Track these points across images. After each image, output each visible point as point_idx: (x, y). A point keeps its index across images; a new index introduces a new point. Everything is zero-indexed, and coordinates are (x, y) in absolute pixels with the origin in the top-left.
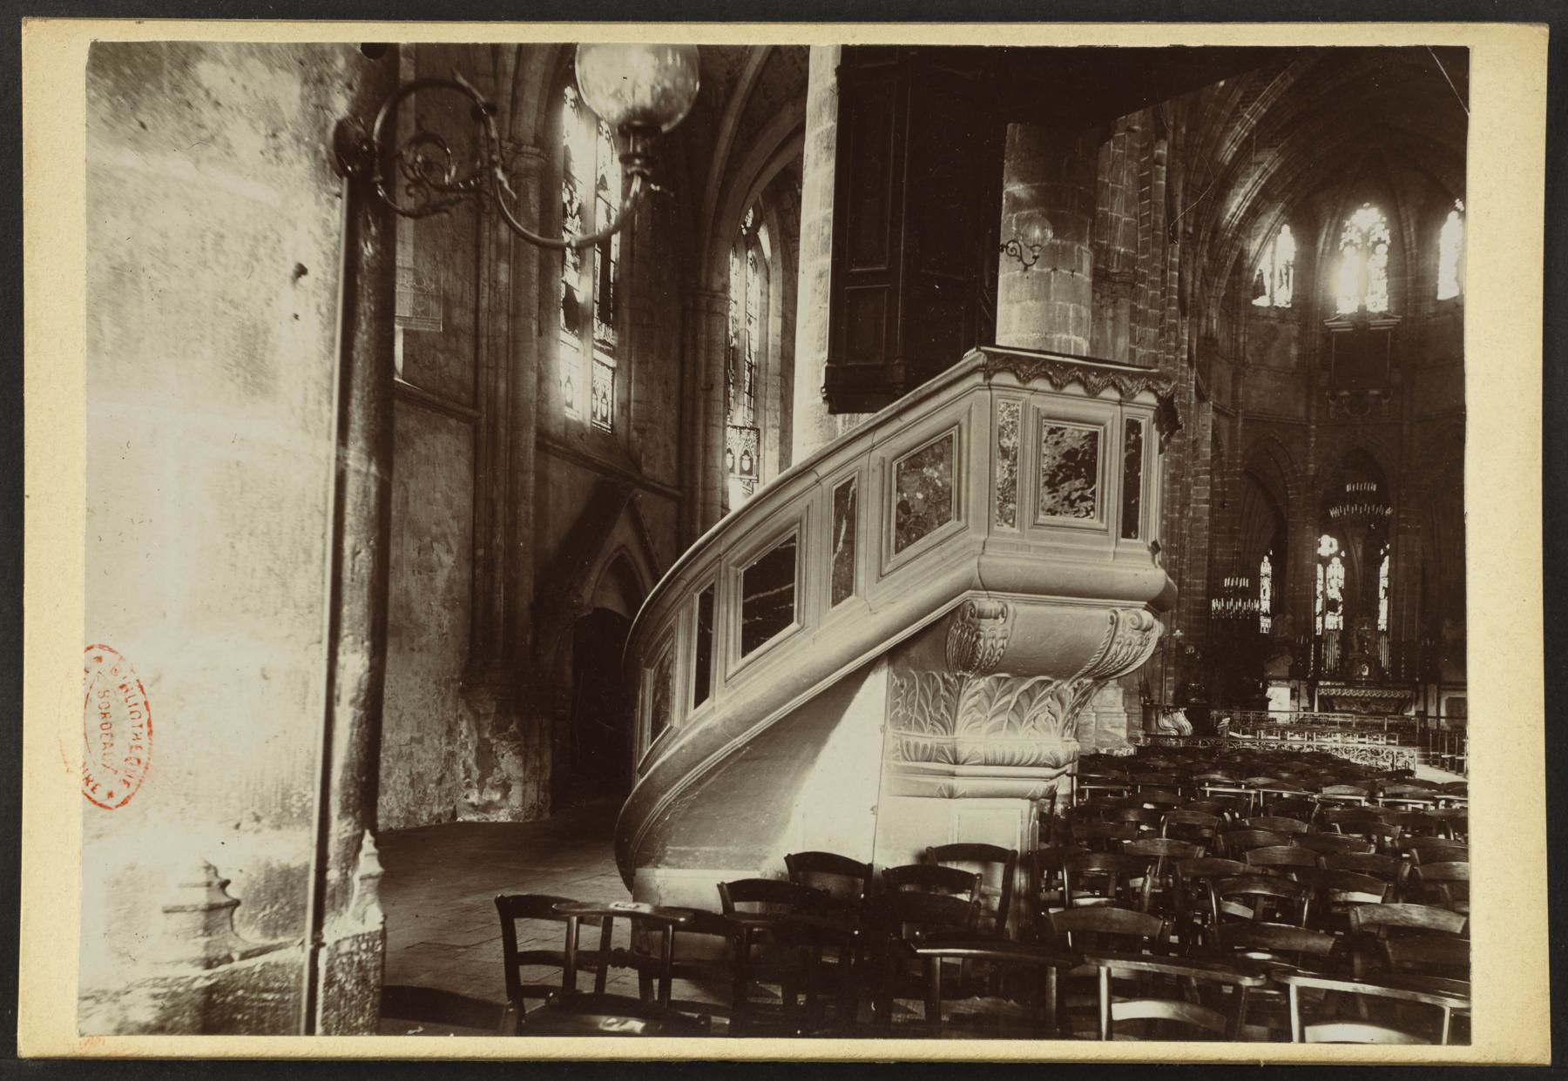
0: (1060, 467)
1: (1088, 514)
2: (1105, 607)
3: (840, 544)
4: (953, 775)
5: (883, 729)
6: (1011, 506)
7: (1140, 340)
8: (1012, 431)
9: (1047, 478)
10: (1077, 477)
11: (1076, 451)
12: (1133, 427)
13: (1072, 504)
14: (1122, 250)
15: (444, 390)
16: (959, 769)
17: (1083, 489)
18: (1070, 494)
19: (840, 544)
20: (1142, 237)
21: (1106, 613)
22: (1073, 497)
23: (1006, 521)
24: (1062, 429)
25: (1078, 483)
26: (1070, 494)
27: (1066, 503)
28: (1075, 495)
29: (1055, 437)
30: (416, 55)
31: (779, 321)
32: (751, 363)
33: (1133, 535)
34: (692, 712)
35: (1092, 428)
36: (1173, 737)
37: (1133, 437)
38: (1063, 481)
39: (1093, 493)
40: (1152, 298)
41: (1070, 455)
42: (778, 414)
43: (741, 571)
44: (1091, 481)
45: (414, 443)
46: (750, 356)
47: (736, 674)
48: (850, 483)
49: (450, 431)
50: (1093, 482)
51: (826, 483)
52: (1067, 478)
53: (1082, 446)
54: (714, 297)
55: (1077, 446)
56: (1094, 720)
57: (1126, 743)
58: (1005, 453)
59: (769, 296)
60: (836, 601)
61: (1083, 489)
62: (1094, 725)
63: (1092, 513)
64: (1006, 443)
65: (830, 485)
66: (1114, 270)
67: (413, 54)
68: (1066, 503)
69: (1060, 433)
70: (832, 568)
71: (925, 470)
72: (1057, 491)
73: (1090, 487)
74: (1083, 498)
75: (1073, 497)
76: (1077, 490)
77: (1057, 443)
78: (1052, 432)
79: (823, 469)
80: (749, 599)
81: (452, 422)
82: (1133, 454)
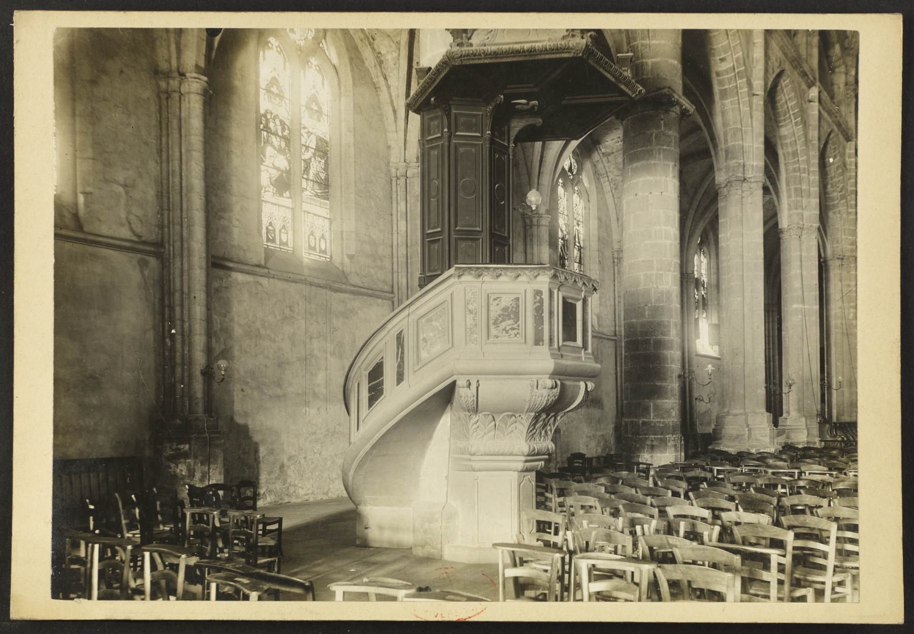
0: (499, 316)
1: (516, 336)
2: (527, 379)
3: (399, 359)
4: (470, 460)
5: (450, 440)
6: (475, 336)
7: (806, 207)
8: (474, 301)
9: (493, 321)
10: (509, 319)
11: (508, 308)
12: (538, 293)
13: (507, 332)
14: (755, 164)
15: (375, 286)
16: (473, 458)
17: (513, 324)
18: (505, 328)
19: (399, 359)
20: (800, 147)
21: (529, 382)
22: (507, 329)
23: (473, 343)
24: (499, 298)
25: (511, 322)
26: (505, 328)
27: (504, 332)
28: (508, 328)
29: (496, 302)
30: (354, 130)
31: (596, 222)
32: (580, 246)
33: (541, 344)
34: (356, 434)
35: (517, 296)
36: (838, 441)
37: (538, 298)
38: (501, 322)
39: (518, 326)
40: (813, 181)
41: (505, 309)
42: (598, 272)
43: (367, 373)
44: (517, 319)
45: (357, 313)
46: (579, 243)
47: (367, 416)
48: (402, 331)
49: (378, 305)
50: (518, 320)
51: (392, 332)
52: (504, 320)
53: (511, 305)
54: (541, 217)
55: (508, 305)
56: (747, 432)
57: (769, 445)
58: (471, 312)
59: (589, 209)
60: (398, 384)
61: (513, 324)
62: (747, 435)
63: (518, 335)
64: (471, 307)
65: (394, 333)
66: (750, 176)
67: (352, 130)
68: (504, 332)
69: (499, 300)
70: (396, 369)
71: (433, 323)
72: (499, 327)
73: (516, 323)
74: (513, 329)
75: (507, 329)
76: (509, 325)
77: (498, 304)
78: (495, 300)
79: (390, 326)
80: (371, 384)
81: (380, 301)
82: (539, 306)
